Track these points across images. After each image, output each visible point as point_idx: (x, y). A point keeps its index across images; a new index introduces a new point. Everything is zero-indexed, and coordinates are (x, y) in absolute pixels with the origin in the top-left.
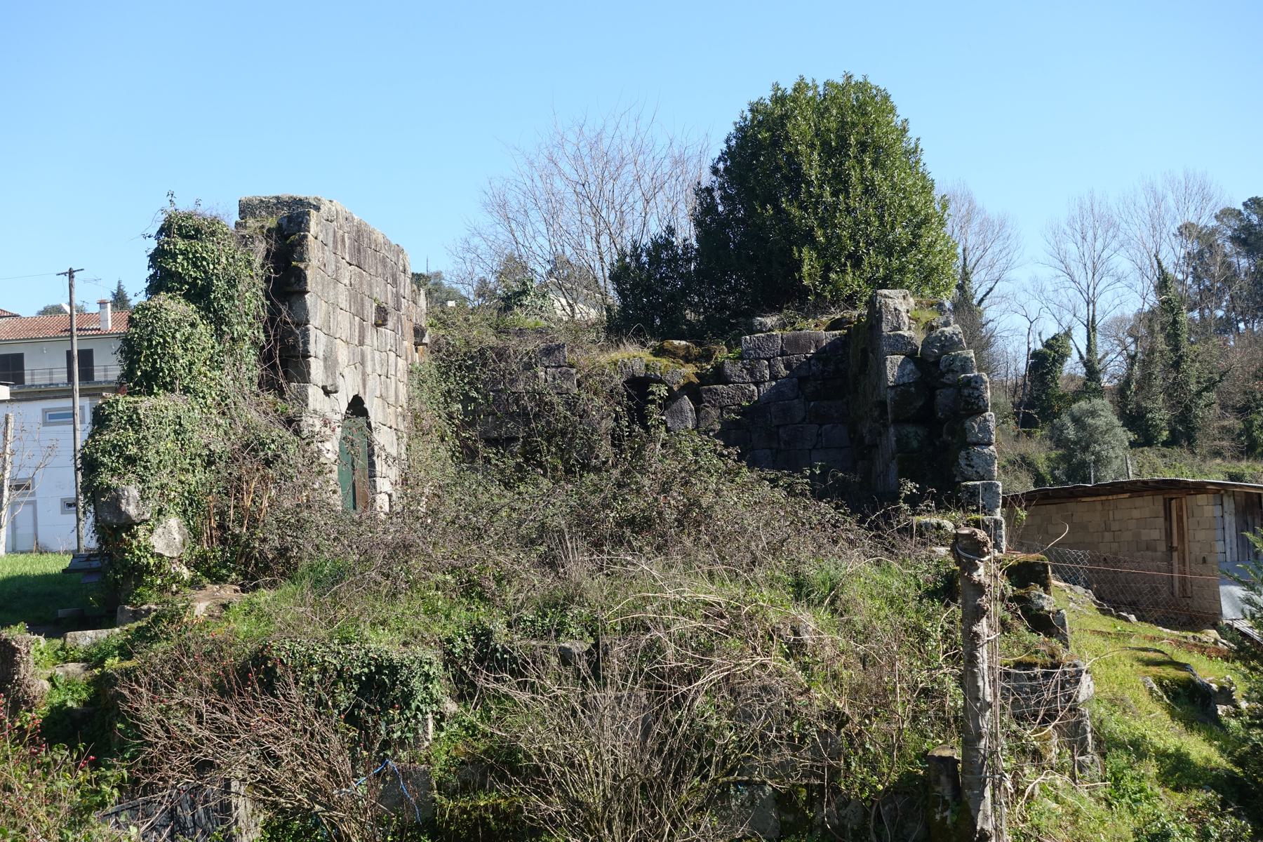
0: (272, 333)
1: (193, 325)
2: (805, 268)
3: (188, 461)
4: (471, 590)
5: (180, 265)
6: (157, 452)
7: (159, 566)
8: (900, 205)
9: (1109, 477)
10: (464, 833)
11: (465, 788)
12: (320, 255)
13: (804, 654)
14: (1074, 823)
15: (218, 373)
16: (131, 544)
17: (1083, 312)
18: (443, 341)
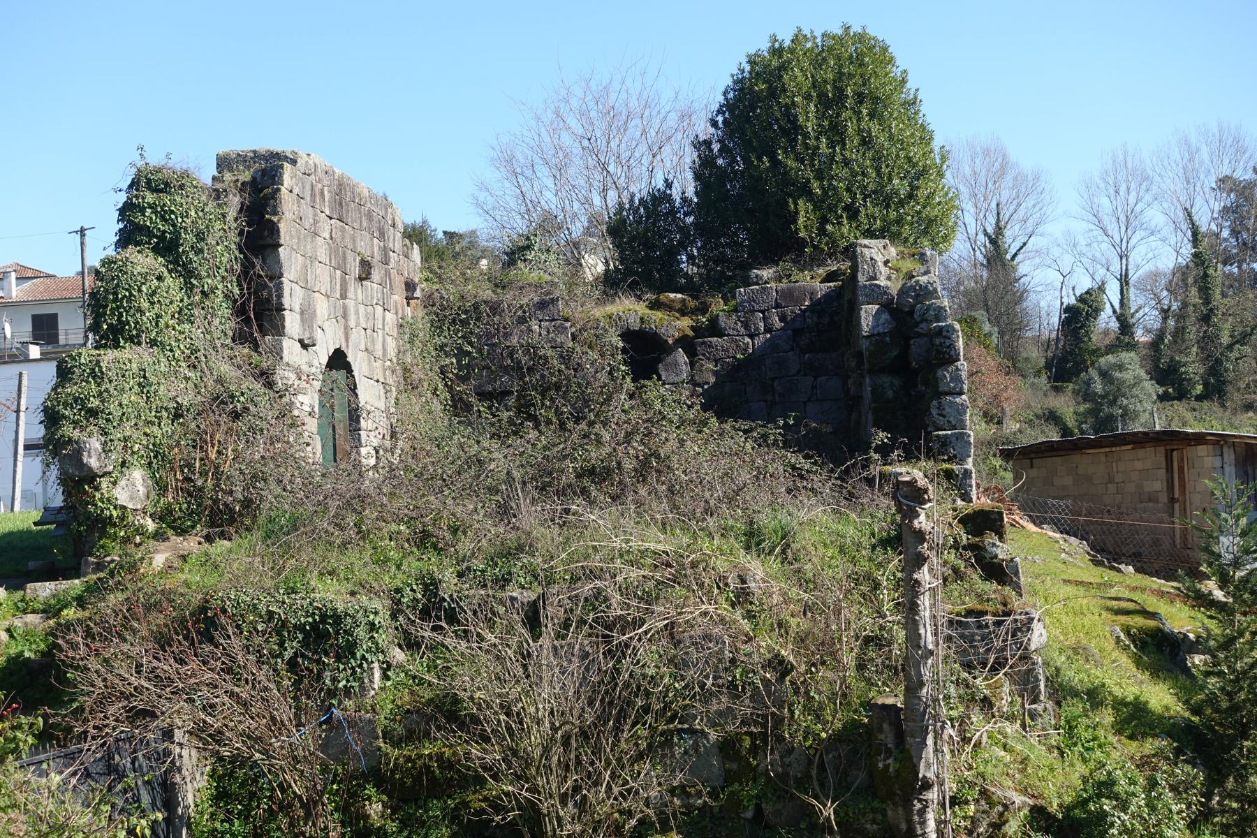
0: (245, 286)
1: (160, 278)
2: (801, 220)
3: (153, 413)
4: (423, 540)
5: (148, 218)
6: (120, 405)
7: (122, 518)
8: (898, 156)
9: (1137, 427)
10: (409, 782)
11: (411, 736)
12: (295, 208)
13: (751, 603)
14: (1023, 771)
15: (187, 326)
16: (94, 496)
17: (1116, 267)
18: (436, 294)
